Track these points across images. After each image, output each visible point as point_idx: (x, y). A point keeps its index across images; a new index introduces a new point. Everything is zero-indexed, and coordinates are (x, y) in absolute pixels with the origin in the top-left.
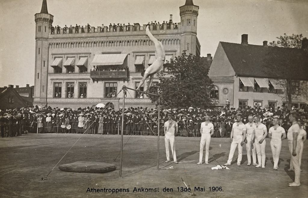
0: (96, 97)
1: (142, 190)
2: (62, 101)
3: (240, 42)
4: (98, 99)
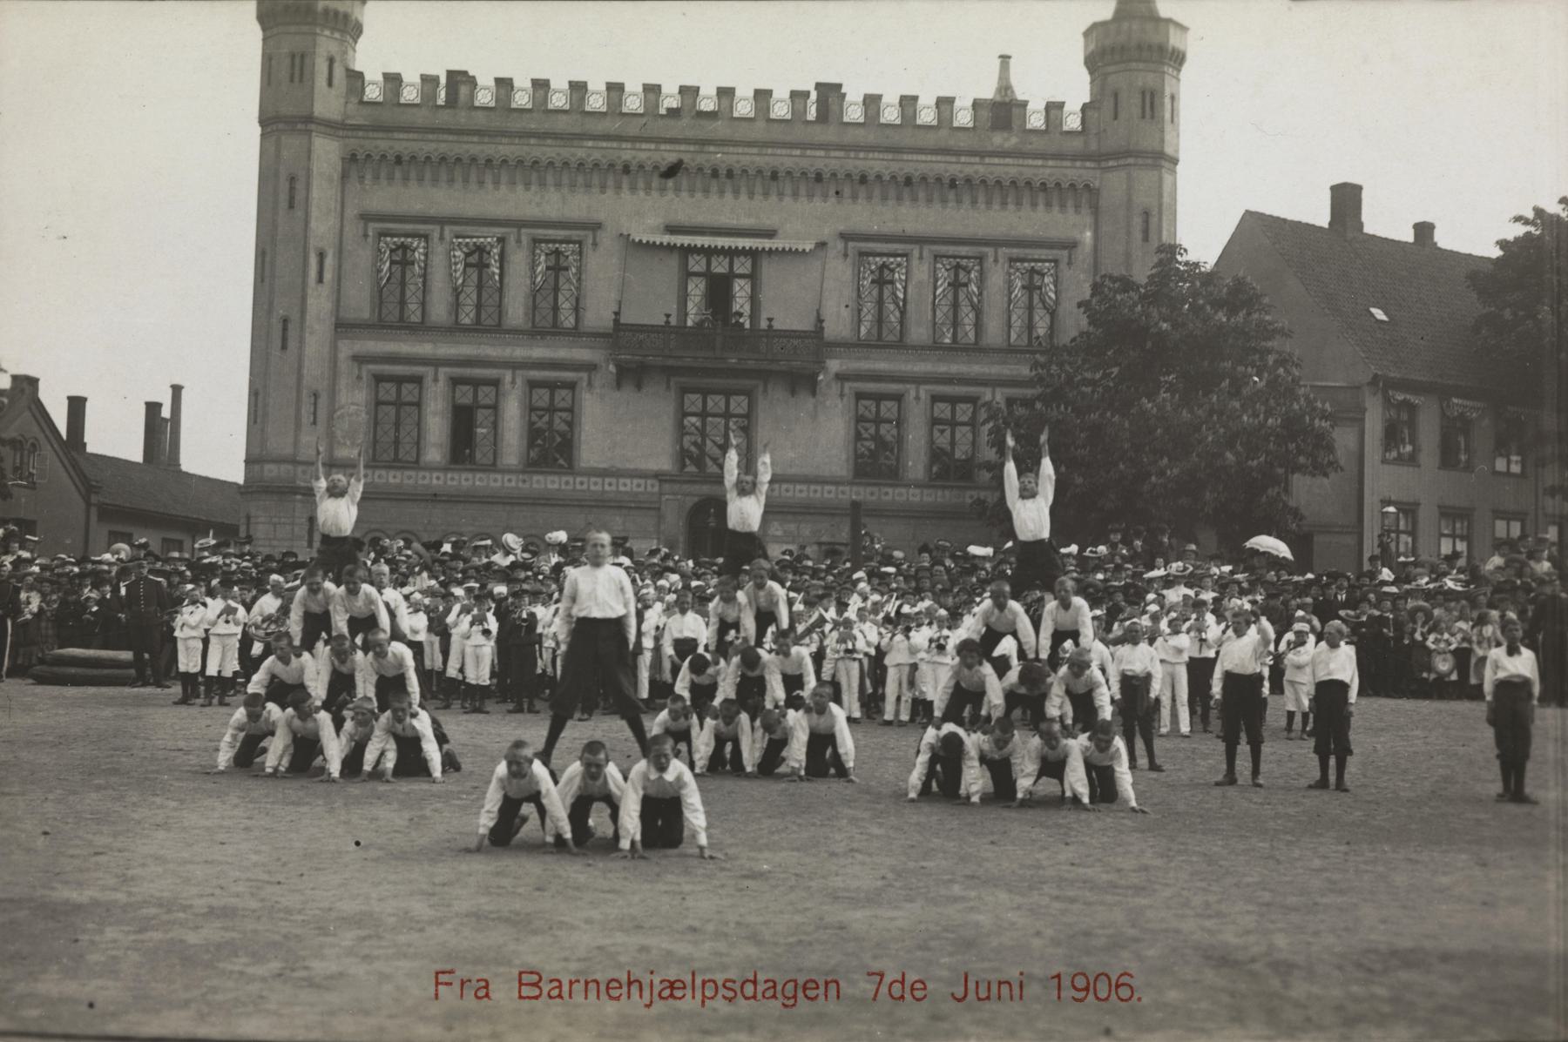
0: (631, 466)
2: (426, 482)
3: (1322, 218)
4: (643, 475)
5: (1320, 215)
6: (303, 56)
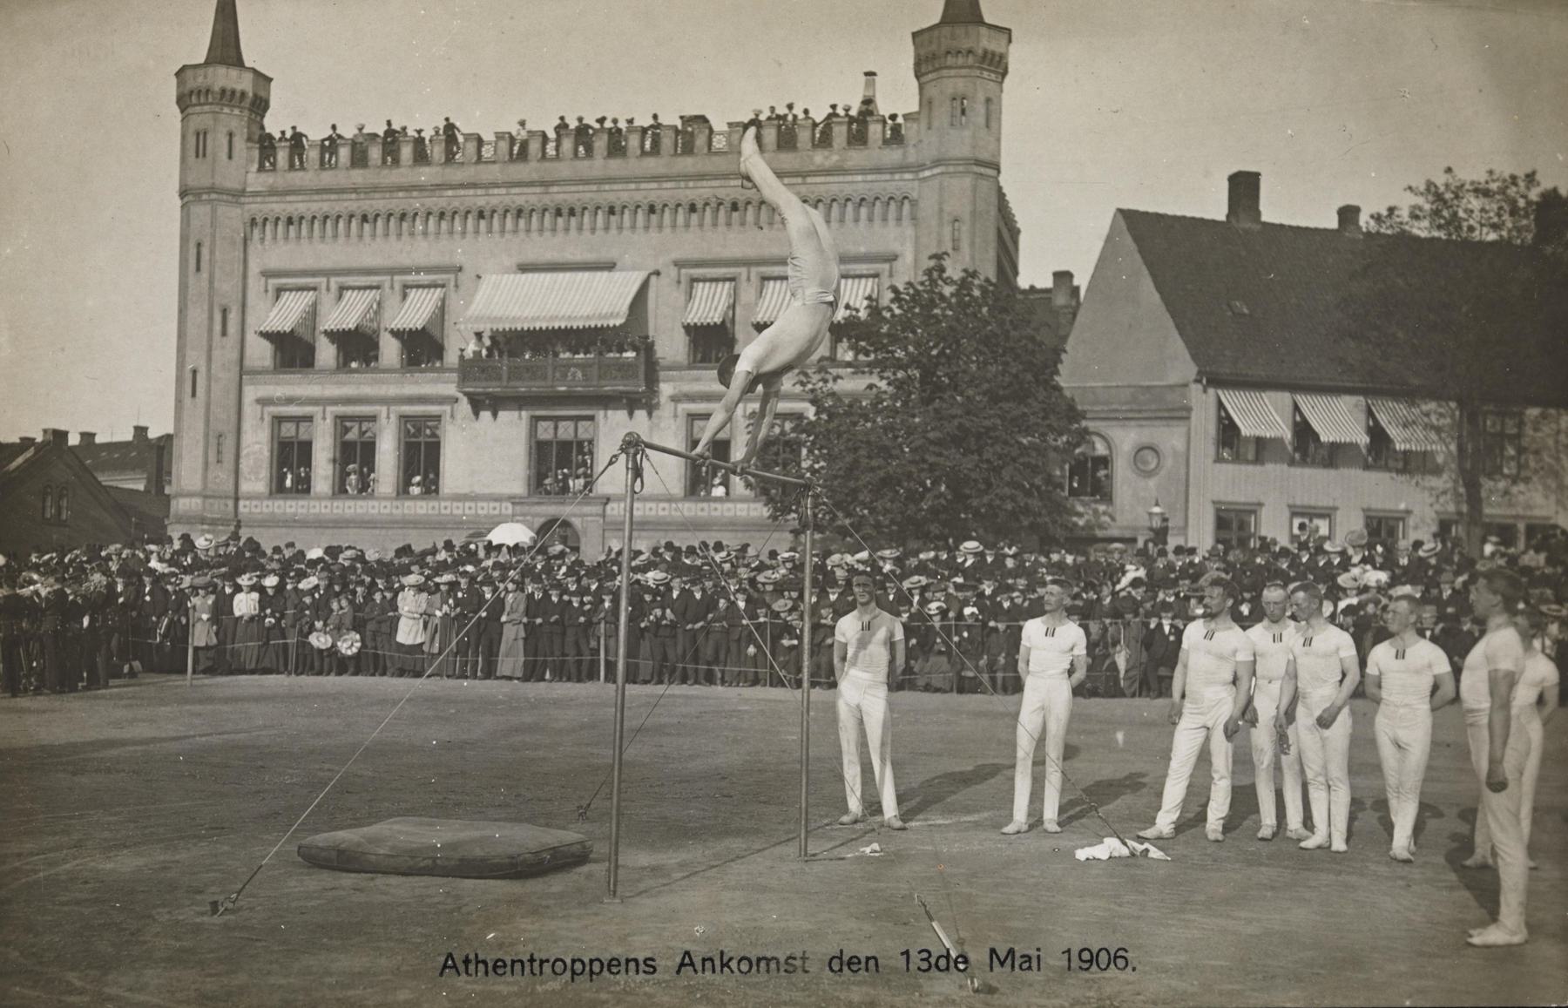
0: (487, 491)
1: (723, 966)
4: (498, 499)
5: (1216, 208)
6: (205, 133)
